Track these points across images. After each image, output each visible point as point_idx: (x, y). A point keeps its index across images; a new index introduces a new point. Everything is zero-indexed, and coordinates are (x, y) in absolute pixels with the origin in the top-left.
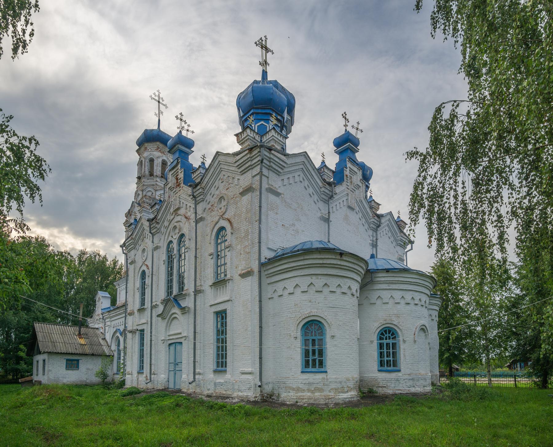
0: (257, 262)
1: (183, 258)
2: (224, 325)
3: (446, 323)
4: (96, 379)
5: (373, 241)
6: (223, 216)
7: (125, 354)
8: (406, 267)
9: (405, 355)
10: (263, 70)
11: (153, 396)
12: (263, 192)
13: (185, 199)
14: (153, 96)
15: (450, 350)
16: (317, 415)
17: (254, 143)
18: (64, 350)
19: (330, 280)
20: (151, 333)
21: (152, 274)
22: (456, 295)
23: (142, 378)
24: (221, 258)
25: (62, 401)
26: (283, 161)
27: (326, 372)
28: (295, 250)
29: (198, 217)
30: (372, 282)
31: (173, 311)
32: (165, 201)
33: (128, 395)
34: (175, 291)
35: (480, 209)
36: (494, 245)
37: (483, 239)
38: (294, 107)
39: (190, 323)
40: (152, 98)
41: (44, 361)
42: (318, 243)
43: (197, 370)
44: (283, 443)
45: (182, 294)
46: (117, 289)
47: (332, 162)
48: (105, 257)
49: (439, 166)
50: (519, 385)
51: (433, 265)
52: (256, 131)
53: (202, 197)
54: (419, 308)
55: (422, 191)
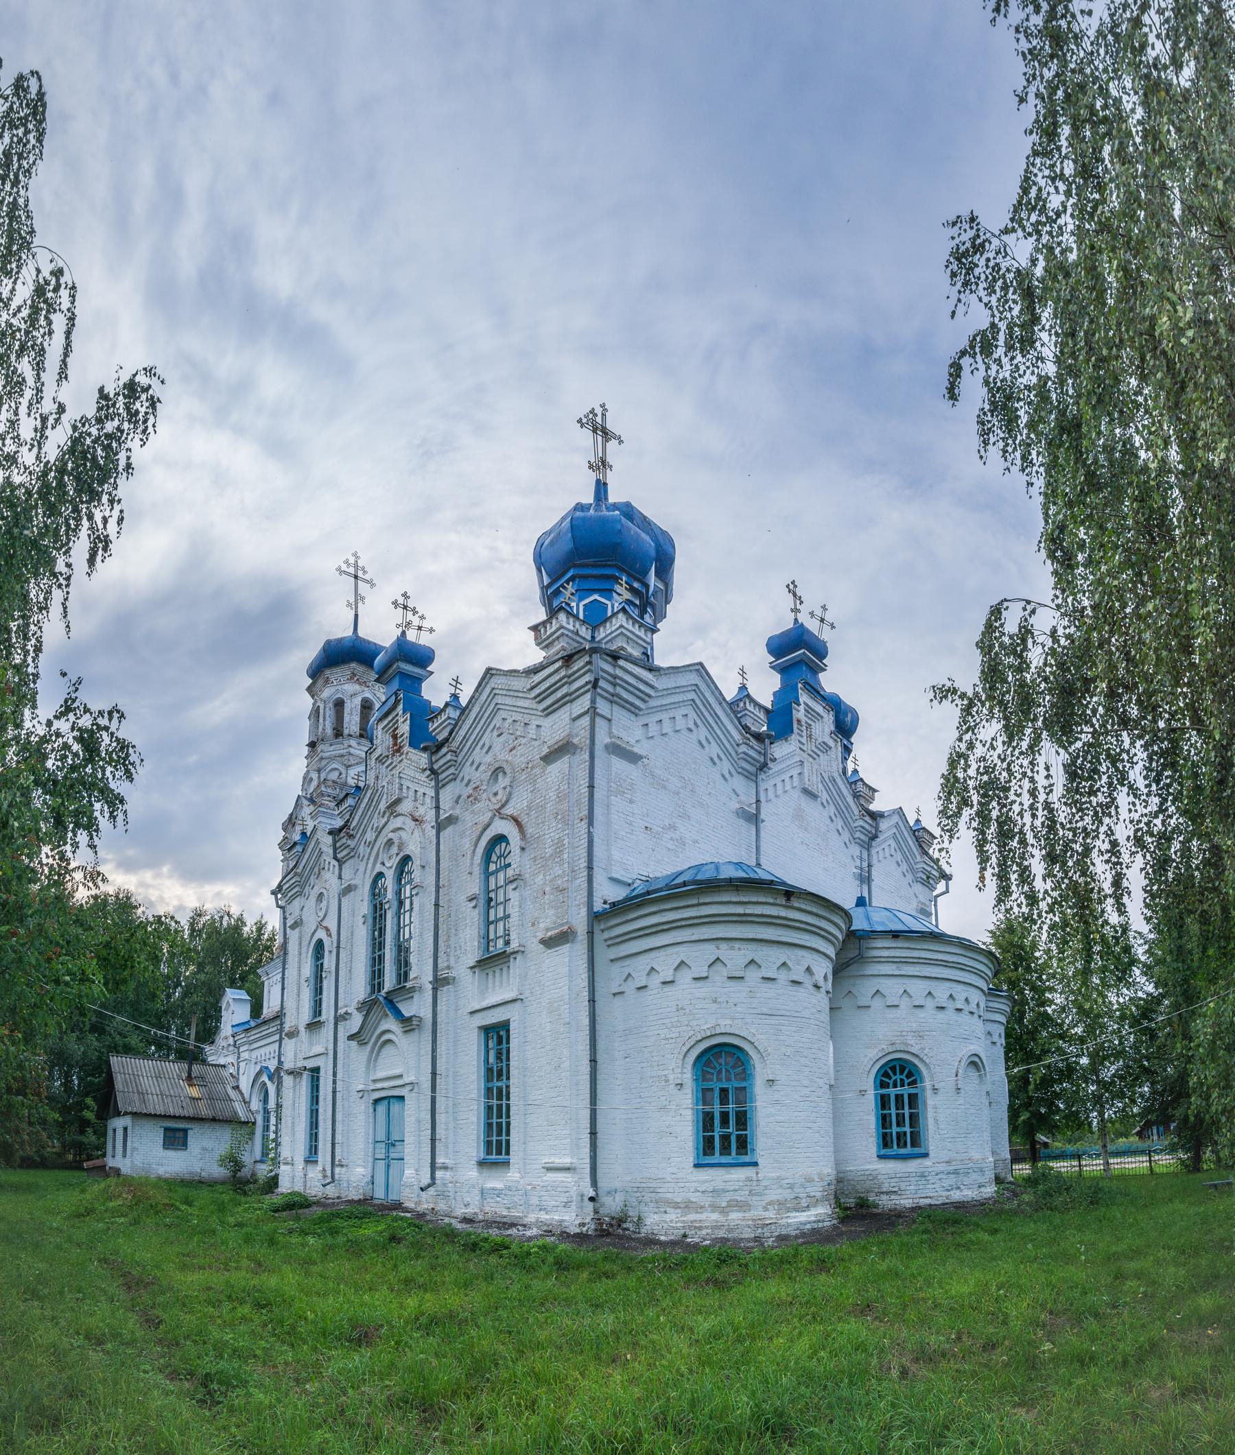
0: (584, 912)
1: (407, 907)
2: (504, 1058)
3: (1021, 1049)
4: (219, 1172)
5: (861, 869)
6: (502, 811)
7: (279, 1118)
8: (936, 930)
9: (936, 1121)
10: (598, 481)
11: (337, 1215)
12: (597, 753)
13: (413, 780)
14: (344, 567)
15: (1030, 1105)
16: (736, 1266)
17: (576, 645)
18: (160, 1110)
19: (760, 953)
20: (335, 1074)
21: (338, 947)
22: (1039, 991)
23: (315, 1173)
24: (497, 905)
25: (157, 1213)
26: (646, 683)
27: (755, 1164)
28: (676, 882)
29: (442, 817)
30: (861, 959)
31: (385, 1025)
32: (367, 787)
33: (284, 1210)
34: (389, 982)
35: (1080, 825)
36: (1105, 897)
37: (1087, 884)
38: (671, 560)
39: (422, 1052)
40: (341, 572)
41: (125, 1129)
42: (732, 867)
43: (440, 1160)
44: (651, 1336)
45: (403, 988)
46: (263, 983)
47: (765, 688)
48: (240, 920)
49: (1000, 726)
50: (1157, 1170)
51: (992, 928)
52: (581, 617)
53: (452, 770)
54: (964, 1017)
55: (965, 771)
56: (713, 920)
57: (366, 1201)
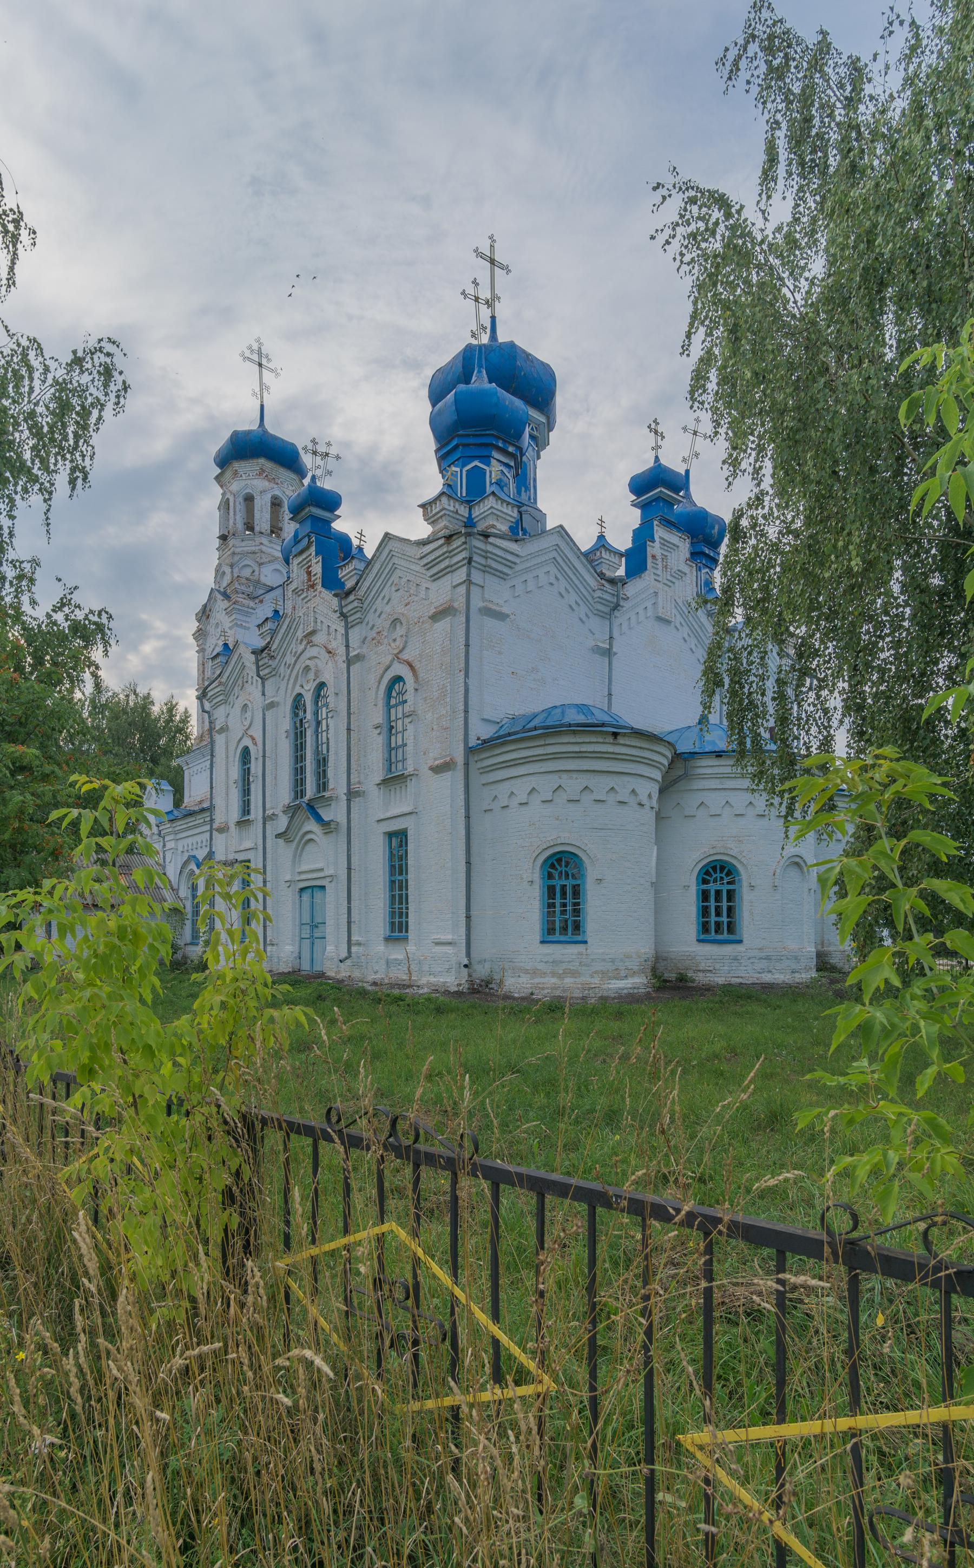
1: (324, 728)
14: (248, 354)
19: (592, 781)
21: (264, 756)
27: (586, 942)
28: (532, 725)
29: (351, 654)
30: (686, 776)
31: (307, 827)
34: (310, 790)
42: (574, 711)
43: (354, 938)
56: (556, 757)
57: (296, 972)
